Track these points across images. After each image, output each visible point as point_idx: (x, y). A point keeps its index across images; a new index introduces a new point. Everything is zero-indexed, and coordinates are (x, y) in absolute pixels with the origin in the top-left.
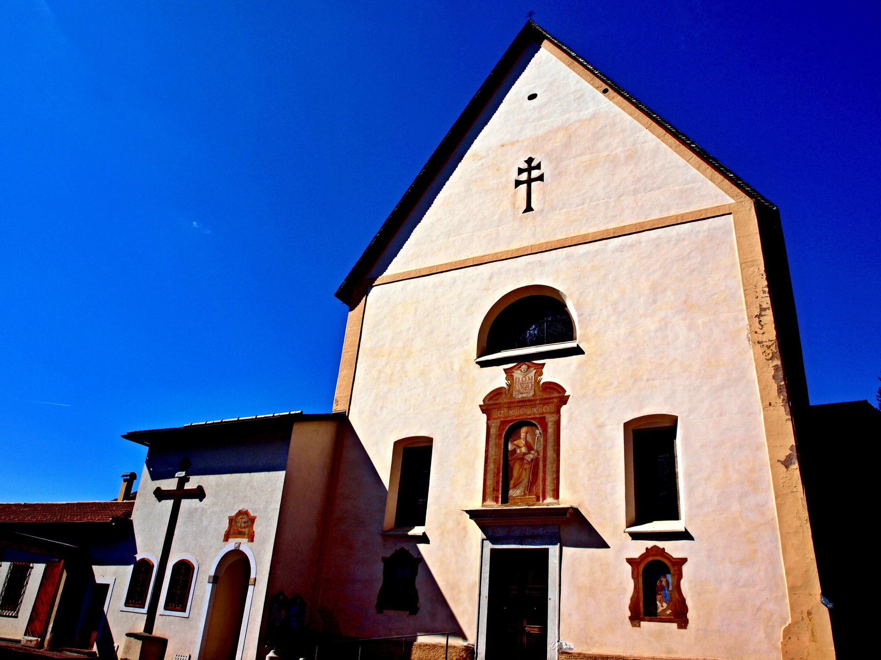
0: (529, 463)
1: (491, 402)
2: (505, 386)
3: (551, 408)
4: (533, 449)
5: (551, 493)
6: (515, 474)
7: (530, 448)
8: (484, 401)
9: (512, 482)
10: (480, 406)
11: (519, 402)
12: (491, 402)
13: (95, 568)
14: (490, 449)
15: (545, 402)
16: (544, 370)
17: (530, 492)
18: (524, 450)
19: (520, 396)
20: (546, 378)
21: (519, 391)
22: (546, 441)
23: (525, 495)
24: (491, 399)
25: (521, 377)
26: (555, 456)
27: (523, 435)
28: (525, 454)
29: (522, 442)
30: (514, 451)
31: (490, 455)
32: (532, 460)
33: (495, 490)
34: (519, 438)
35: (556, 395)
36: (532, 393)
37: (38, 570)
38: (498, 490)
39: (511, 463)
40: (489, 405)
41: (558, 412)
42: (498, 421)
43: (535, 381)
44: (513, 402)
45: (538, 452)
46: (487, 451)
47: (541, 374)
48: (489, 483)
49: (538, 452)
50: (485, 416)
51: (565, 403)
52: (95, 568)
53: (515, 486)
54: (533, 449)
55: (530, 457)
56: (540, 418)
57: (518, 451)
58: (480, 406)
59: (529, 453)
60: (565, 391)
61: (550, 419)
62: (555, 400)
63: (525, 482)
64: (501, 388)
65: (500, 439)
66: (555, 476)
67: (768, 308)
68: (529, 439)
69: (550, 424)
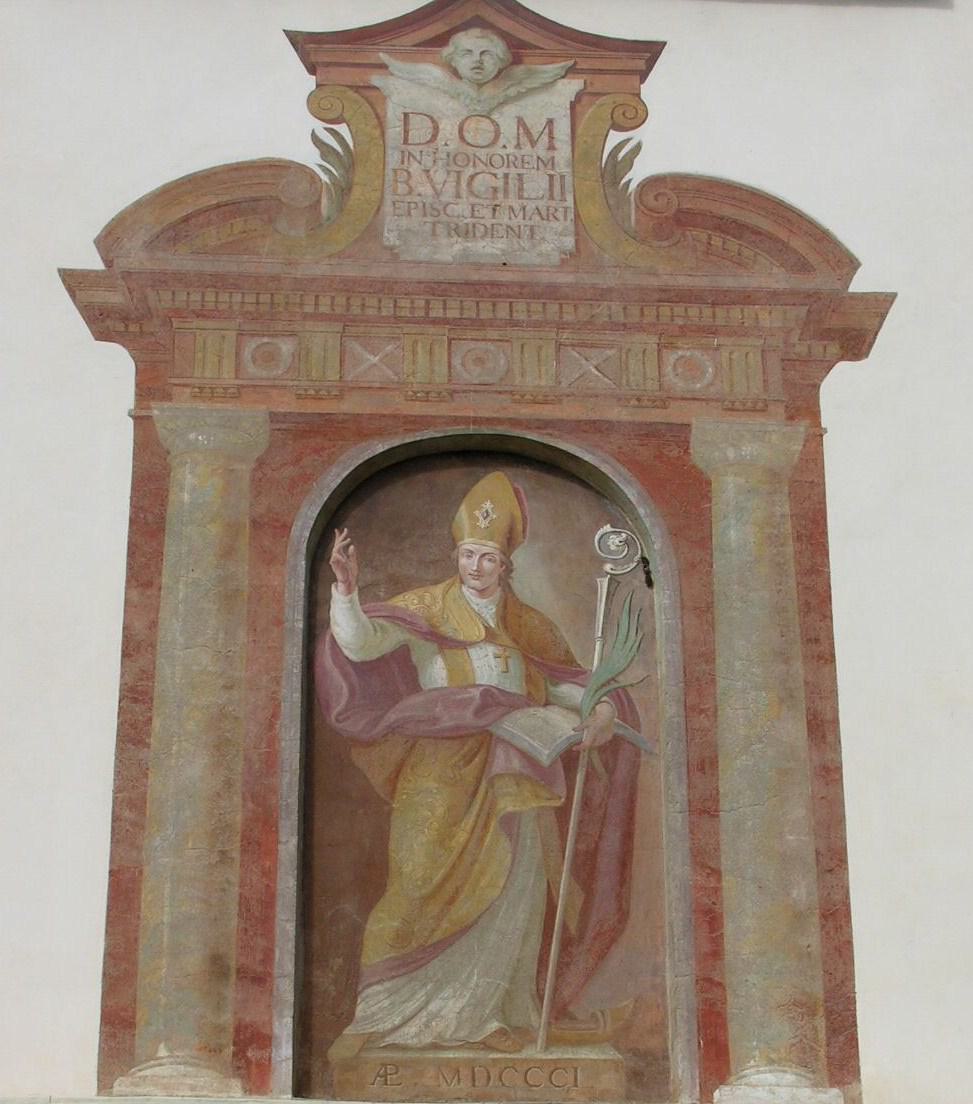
0: (534, 772)
1: (180, 260)
2: (310, 157)
3: (739, 365)
4: (566, 668)
5: (783, 1030)
6: (413, 852)
7: (546, 663)
8: (109, 240)
9: (381, 927)
10: (74, 281)
11: (439, 289)
12: (180, 260)
13: (851, 290)
14: (172, 629)
15: (682, 315)
16: (652, 90)
17: (561, 1012)
18: (487, 666)
19: (450, 250)
20: (685, 130)
21: (434, 210)
22: (700, 609)
23: (518, 1035)
24: (175, 234)
25: (449, 112)
26: (795, 730)
27: (475, 547)
28: (493, 701)
29: (469, 607)
30: (392, 673)
31: (170, 676)
32: (569, 758)
33: (236, 970)
34: (445, 568)
35: (770, 276)
36: (556, 239)
37: (349, 539)
38: (258, 979)
39: (373, 767)
40: (161, 280)
41: (804, 407)
42: (251, 426)
43: (584, 152)
44: (386, 288)
45: (622, 699)
46: (137, 647)
47: (633, 115)
48: (163, 906)
49: (622, 699)
50: (116, 366)
51: (856, 344)
52: (851, 290)
53: (415, 958)
54: (566, 668)
55: (545, 730)
56: (648, 433)
57: (436, 672)
58: (74, 281)
59: (536, 697)
60: (848, 264)
61: (734, 455)
62: (769, 318)
63: (511, 931)
64: (276, 168)
65: (269, 558)
66: (803, 891)
67: (478, 315)
68: (533, 582)
69: (728, 490)
